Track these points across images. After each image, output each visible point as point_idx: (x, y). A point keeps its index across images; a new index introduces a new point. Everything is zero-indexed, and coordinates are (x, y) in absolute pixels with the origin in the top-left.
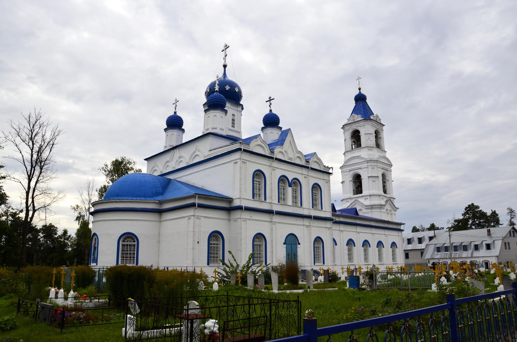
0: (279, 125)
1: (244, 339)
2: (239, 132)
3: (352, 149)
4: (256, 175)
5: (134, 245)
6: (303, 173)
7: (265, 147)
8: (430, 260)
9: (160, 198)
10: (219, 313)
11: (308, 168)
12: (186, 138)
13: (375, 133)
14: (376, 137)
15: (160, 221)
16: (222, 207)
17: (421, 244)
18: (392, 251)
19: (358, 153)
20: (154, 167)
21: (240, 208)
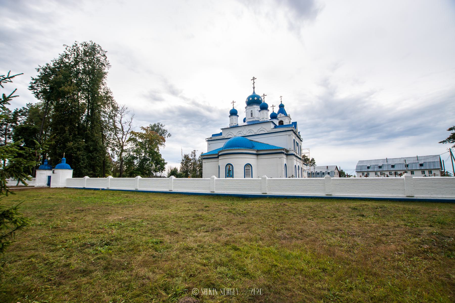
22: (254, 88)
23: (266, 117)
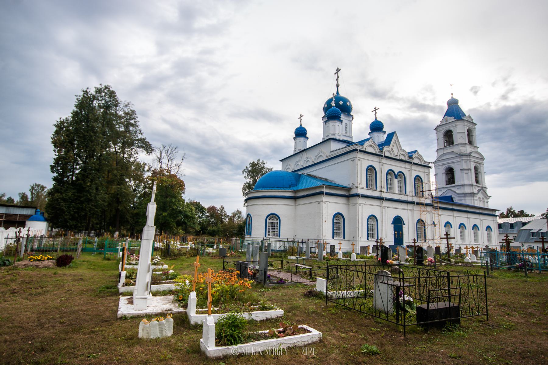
0: (383, 129)
1: (426, 308)
2: (351, 137)
3: (445, 146)
4: (369, 169)
5: (277, 223)
6: (407, 167)
7: (375, 147)
8: (523, 244)
9: (295, 188)
10: (363, 280)
11: (411, 163)
12: (309, 144)
13: (468, 131)
14: (468, 135)
15: (295, 206)
16: (340, 194)
17: (513, 229)
18: (473, 233)
19: (449, 150)
20: (287, 166)
21: (357, 195)
22: (338, 86)
23: (332, 132)
